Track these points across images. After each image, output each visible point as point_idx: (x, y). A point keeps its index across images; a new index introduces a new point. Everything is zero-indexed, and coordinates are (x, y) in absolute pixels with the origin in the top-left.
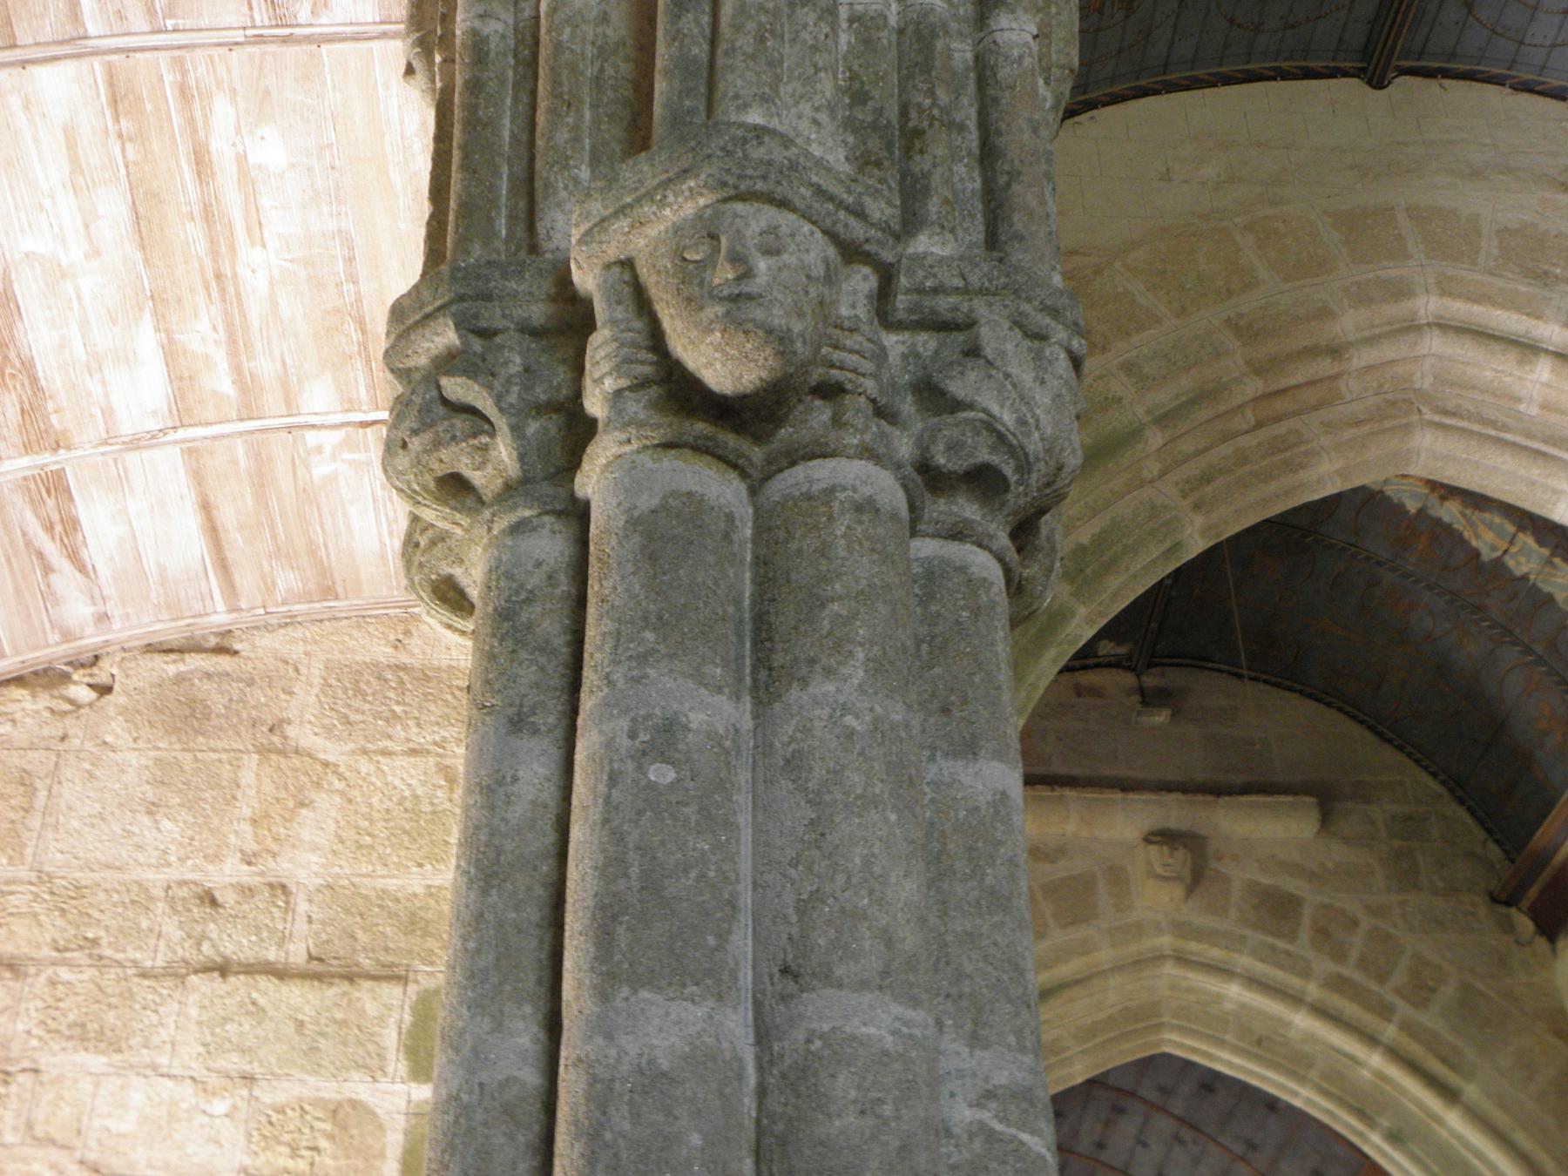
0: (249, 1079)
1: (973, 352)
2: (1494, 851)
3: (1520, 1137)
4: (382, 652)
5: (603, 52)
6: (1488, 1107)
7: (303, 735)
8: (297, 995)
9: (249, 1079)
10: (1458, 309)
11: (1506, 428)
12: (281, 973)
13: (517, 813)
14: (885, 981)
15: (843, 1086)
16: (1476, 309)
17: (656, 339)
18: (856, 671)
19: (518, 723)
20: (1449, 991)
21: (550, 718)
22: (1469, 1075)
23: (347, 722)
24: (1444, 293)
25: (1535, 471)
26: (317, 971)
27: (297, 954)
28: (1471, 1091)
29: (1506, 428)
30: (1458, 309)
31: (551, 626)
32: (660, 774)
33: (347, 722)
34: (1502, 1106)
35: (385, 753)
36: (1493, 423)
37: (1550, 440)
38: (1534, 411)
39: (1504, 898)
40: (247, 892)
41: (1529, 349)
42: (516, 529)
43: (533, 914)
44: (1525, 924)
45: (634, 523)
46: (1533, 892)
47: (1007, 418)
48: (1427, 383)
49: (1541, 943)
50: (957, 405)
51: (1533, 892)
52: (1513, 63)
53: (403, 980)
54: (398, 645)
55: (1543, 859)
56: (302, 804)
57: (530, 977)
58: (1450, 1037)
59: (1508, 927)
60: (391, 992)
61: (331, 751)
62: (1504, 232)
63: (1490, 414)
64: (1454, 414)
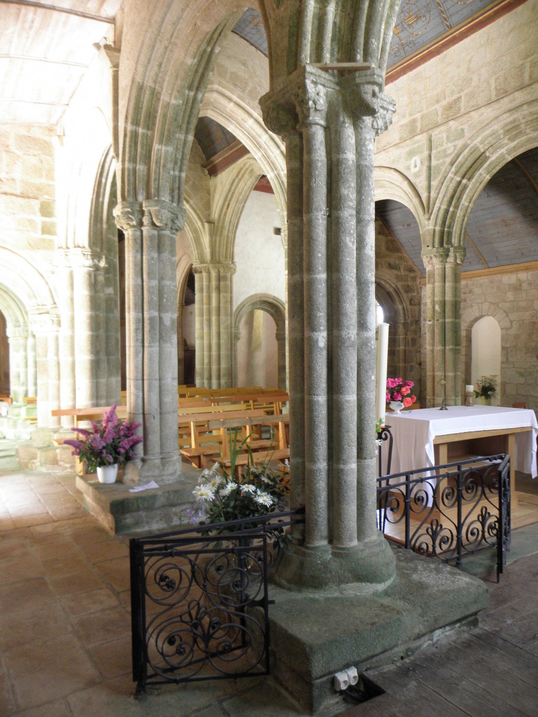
0: (14, 214)
1: (177, 218)
2: (204, 156)
3: (198, 212)
4: (25, 133)
5: (143, 176)
6: (194, 205)
7: (12, 148)
8: (20, 200)
9: (14, 214)
10: (221, 89)
11: (223, 113)
12: (17, 196)
13: (138, 260)
14: (169, 280)
15: (166, 288)
16: (224, 90)
17: (152, 218)
18: (167, 253)
19: (137, 251)
20: (191, 183)
21: (140, 251)
22: (191, 199)
23: (21, 147)
24: (219, 85)
25: (226, 122)
26: (23, 196)
27: (18, 192)
28: (191, 202)
29: (223, 113)
30: (221, 89)
31: (139, 242)
32: (153, 262)
33: (21, 147)
34: (196, 206)
35: (29, 155)
36: (220, 110)
37: (230, 117)
38: (229, 111)
39: (204, 166)
40: (8, 180)
41: (230, 100)
42: (135, 230)
43: (140, 269)
44: (207, 172)
45: (150, 237)
46: (209, 167)
47: (179, 225)
48: (212, 100)
49: (209, 176)
50: (175, 223)
51: (209, 167)
52: (241, 32)
53: (37, 199)
54: (28, 132)
55: (212, 162)
56: (15, 163)
57: (140, 275)
58: (190, 192)
59: (203, 172)
60: (36, 201)
61: (19, 153)
62: (232, 73)
63: (221, 109)
64: (215, 108)
